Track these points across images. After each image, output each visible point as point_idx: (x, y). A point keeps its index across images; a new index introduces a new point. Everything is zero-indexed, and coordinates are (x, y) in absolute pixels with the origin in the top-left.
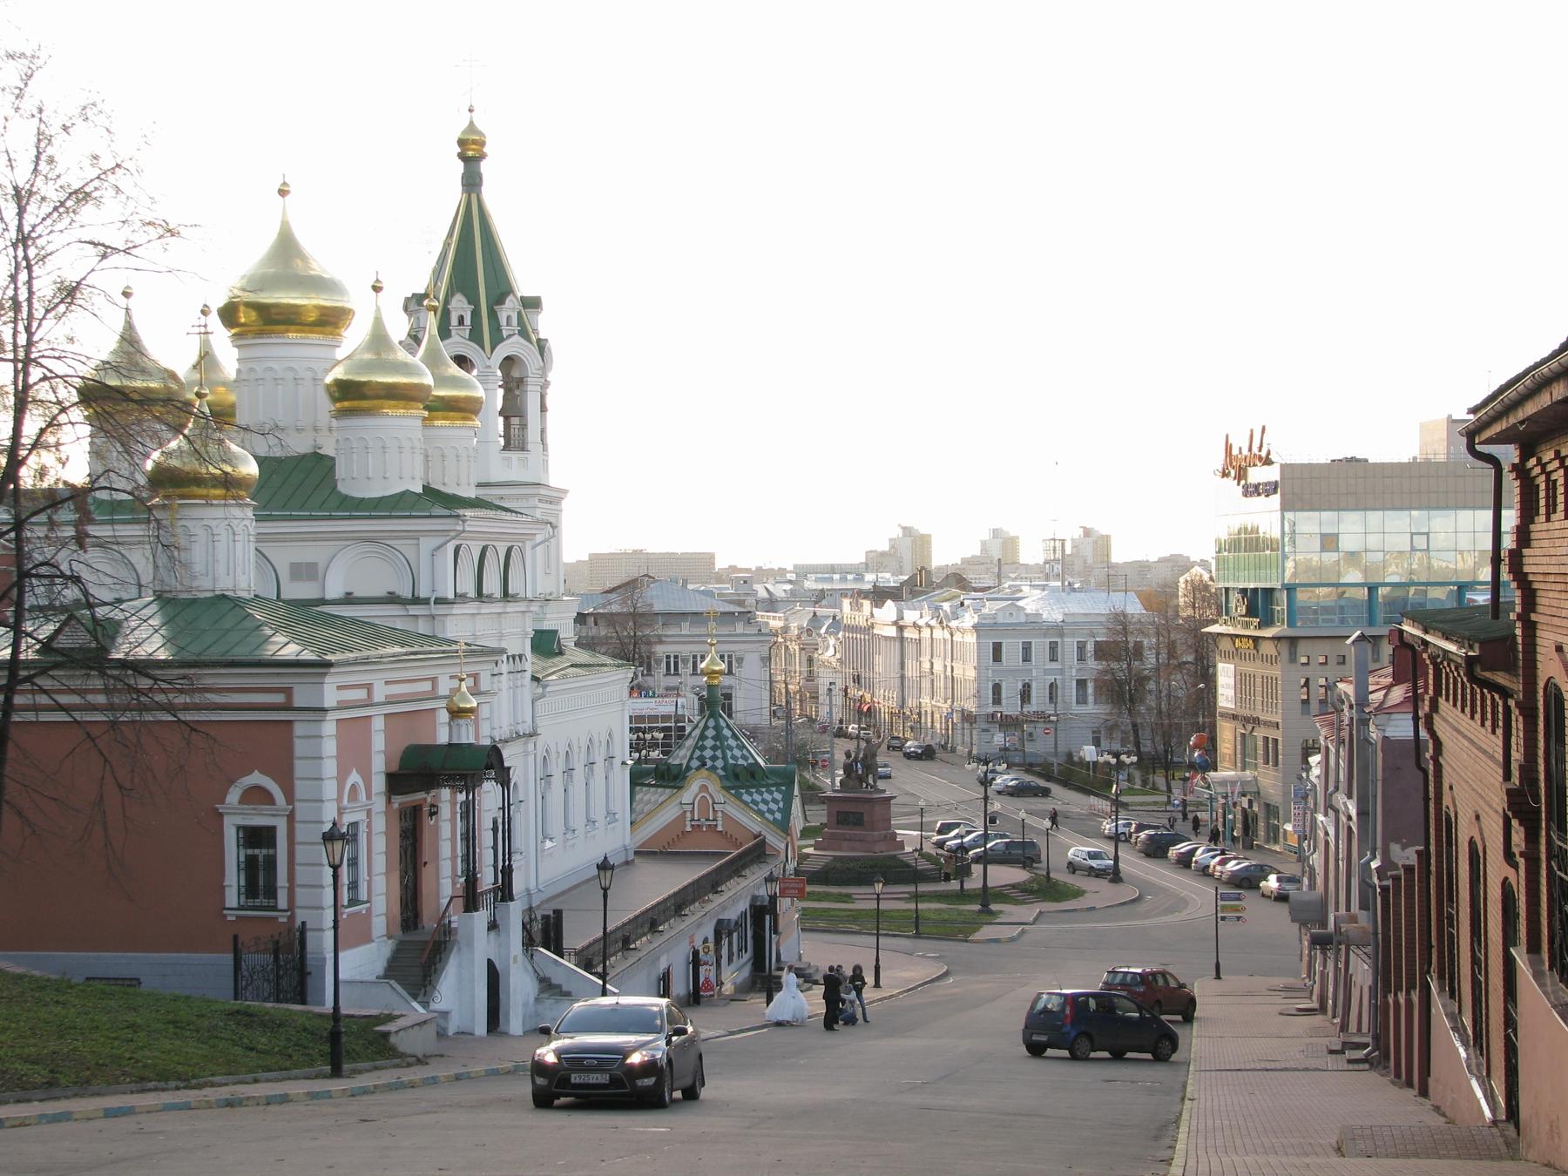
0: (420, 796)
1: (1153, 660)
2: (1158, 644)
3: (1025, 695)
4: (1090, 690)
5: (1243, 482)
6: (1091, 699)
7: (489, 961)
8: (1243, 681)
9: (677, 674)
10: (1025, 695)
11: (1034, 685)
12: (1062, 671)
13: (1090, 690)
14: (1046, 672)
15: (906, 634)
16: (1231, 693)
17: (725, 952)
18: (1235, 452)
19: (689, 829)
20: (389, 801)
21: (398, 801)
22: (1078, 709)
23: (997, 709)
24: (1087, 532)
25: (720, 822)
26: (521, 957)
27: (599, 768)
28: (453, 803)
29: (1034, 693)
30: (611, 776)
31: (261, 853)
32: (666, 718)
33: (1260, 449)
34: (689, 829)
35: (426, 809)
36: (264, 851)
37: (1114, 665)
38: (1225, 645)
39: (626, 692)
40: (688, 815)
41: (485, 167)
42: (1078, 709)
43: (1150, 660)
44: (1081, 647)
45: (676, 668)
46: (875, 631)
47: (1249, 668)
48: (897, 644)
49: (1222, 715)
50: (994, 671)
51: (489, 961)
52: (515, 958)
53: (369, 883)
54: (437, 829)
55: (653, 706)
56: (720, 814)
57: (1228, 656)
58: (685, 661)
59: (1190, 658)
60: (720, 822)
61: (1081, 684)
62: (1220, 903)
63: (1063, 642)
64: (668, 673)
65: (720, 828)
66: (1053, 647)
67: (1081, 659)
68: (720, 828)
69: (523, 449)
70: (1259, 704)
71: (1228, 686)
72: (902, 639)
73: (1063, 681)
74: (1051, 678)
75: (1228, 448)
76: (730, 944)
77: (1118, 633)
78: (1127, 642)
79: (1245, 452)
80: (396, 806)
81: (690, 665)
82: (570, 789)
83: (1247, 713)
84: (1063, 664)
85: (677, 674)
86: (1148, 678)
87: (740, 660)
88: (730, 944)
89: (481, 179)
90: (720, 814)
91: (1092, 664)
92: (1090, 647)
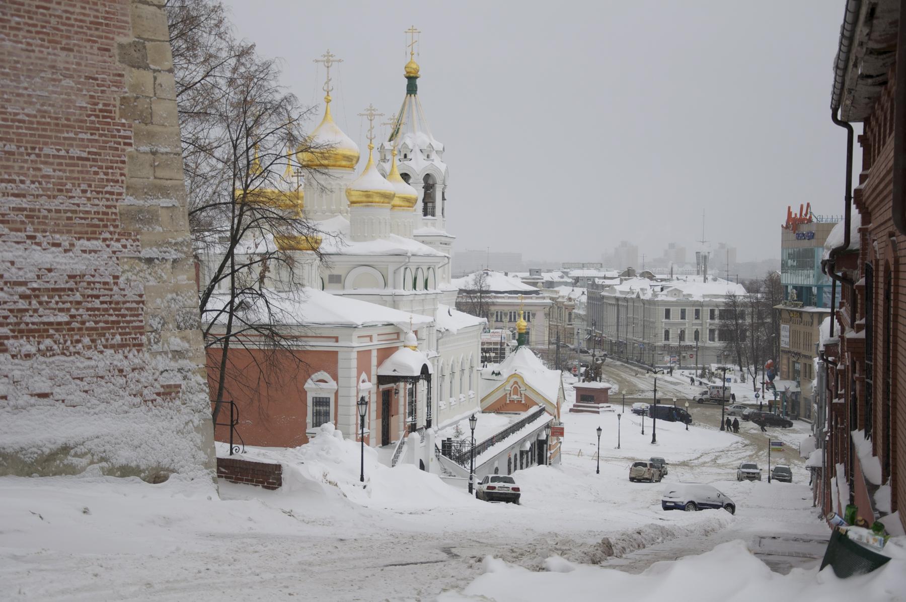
0: (392, 385)
1: (750, 321)
2: (753, 312)
3: (682, 336)
4: (716, 335)
5: (797, 232)
6: (717, 339)
7: (421, 460)
8: (794, 334)
9: (501, 321)
10: (682, 336)
11: (687, 332)
12: (701, 325)
13: (716, 335)
14: (693, 325)
15: (620, 303)
16: (787, 340)
17: (524, 461)
18: (793, 216)
19: (508, 402)
20: (378, 387)
21: (382, 387)
22: (709, 344)
23: (667, 342)
24: (722, 246)
25: (523, 399)
26: (435, 459)
27: (467, 372)
28: (405, 389)
29: (686, 336)
30: (472, 375)
31: (323, 409)
32: (495, 343)
33: (806, 215)
34: (508, 402)
35: (394, 391)
36: (325, 408)
37: (728, 322)
38: (785, 315)
39: (627, 474)
40: (508, 395)
41: (418, 82)
42: (709, 344)
43: (748, 321)
44: (712, 312)
45: (501, 318)
46: (605, 301)
47: (797, 327)
48: (616, 308)
49: (783, 351)
50: (665, 324)
51: (421, 460)
52: (432, 459)
53: (369, 423)
54: (398, 399)
55: (489, 337)
56: (523, 396)
57: (786, 322)
58: (506, 314)
59: (769, 320)
60: (523, 399)
61: (712, 331)
62: (771, 447)
63: (702, 310)
64: (497, 321)
65: (523, 402)
66: (697, 312)
67: (712, 317)
68: (523, 402)
69: (433, 215)
70: (802, 346)
71: (786, 336)
72: (618, 305)
73: (702, 330)
74: (695, 328)
75: (790, 213)
76: (527, 457)
77: (731, 306)
78: (736, 310)
79: (798, 216)
80: (381, 390)
81: (508, 317)
82: (453, 382)
83: (796, 350)
84: (702, 320)
85: (501, 321)
86: (746, 330)
87: (534, 315)
88: (527, 457)
89: (416, 87)
90: (523, 396)
91: (717, 321)
92: (717, 313)
